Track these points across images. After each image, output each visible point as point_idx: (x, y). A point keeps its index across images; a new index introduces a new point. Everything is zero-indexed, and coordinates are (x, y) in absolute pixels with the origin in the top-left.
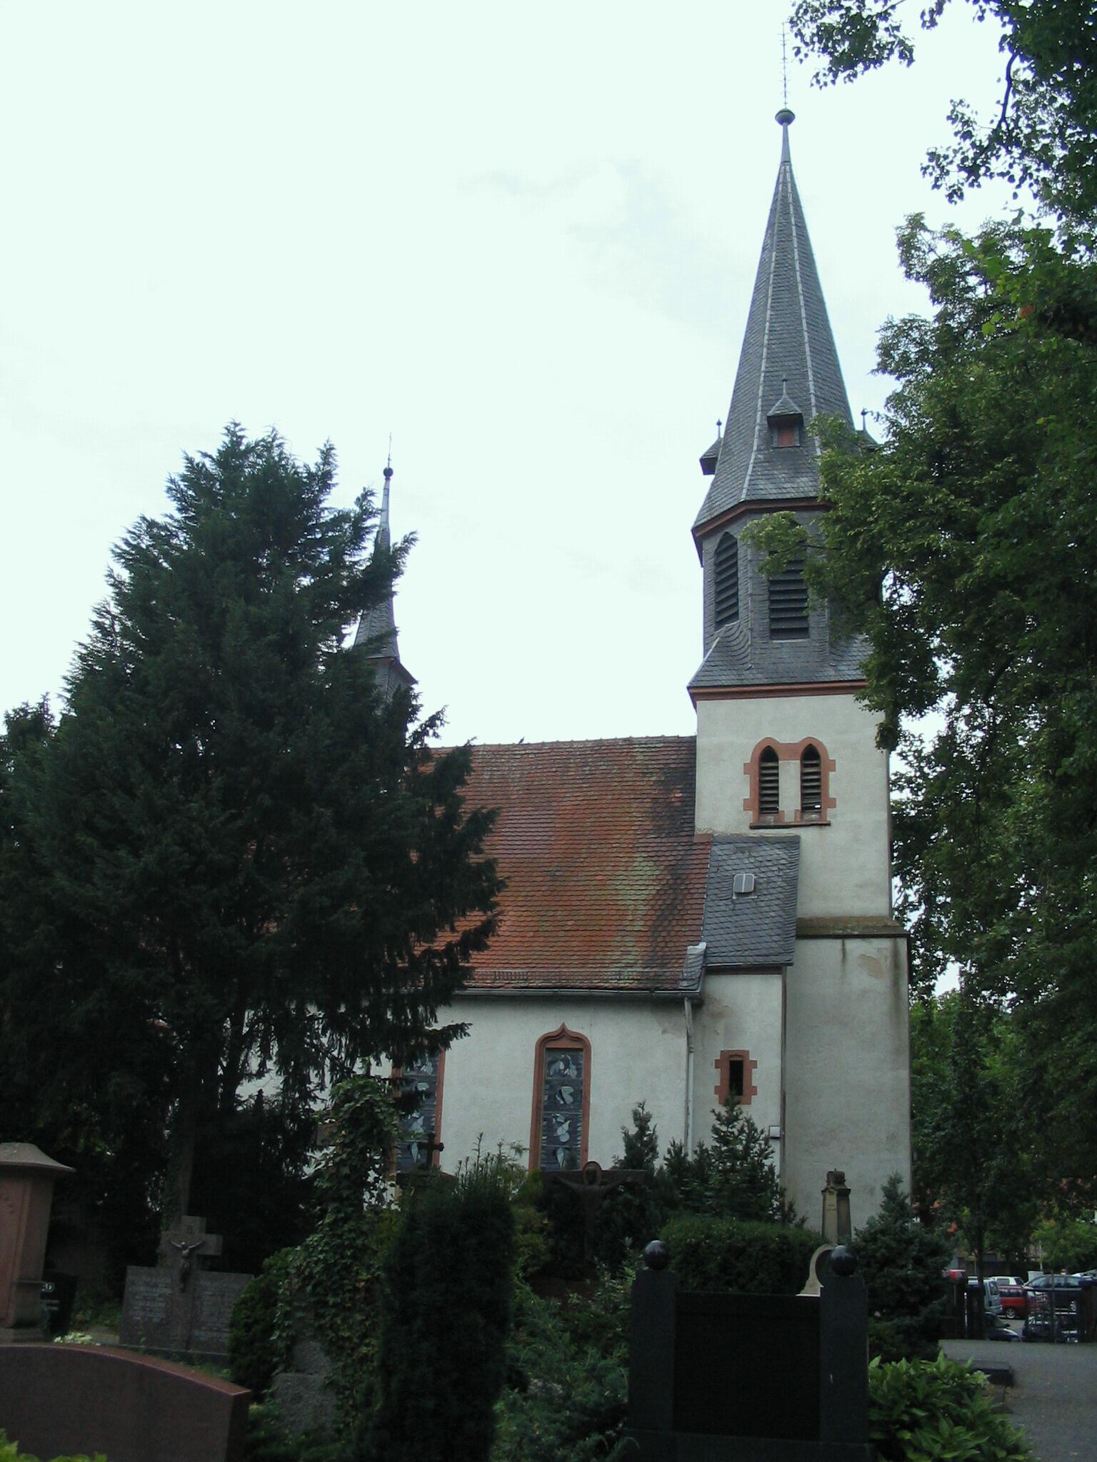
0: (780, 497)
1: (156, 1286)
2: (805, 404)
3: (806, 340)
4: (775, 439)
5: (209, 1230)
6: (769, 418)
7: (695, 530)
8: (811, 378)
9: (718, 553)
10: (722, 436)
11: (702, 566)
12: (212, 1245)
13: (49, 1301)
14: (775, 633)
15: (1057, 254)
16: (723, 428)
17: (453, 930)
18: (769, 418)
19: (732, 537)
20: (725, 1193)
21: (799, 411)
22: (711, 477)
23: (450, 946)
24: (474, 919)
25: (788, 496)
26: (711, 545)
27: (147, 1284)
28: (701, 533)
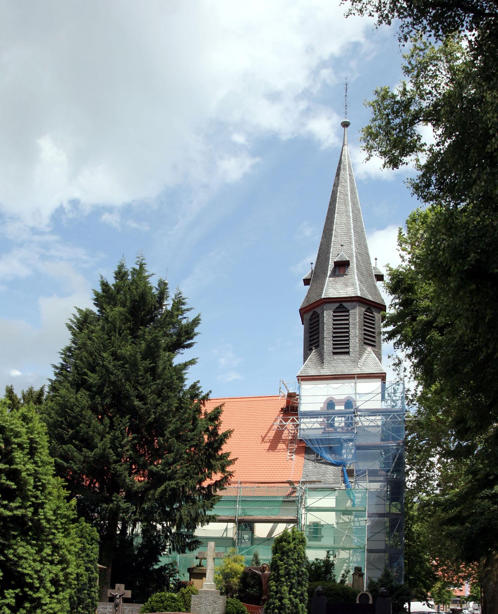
0: (339, 296)
1: (106, 608)
2: (351, 256)
3: (352, 227)
4: (337, 271)
5: (126, 588)
6: (335, 262)
7: (301, 310)
8: (354, 244)
9: (311, 320)
10: (313, 269)
11: (303, 324)
12: (129, 594)
13: (397, 456)
14: (334, 353)
15: (405, 477)
16: (314, 266)
17: (211, 479)
18: (335, 262)
19: (317, 313)
20: (358, 524)
21: (348, 259)
22: (308, 287)
23: (209, 486)
24: (217, 477)
25: (342, 296)
26: (308, 316)
27: (103, 608)
28: (303, 311)
